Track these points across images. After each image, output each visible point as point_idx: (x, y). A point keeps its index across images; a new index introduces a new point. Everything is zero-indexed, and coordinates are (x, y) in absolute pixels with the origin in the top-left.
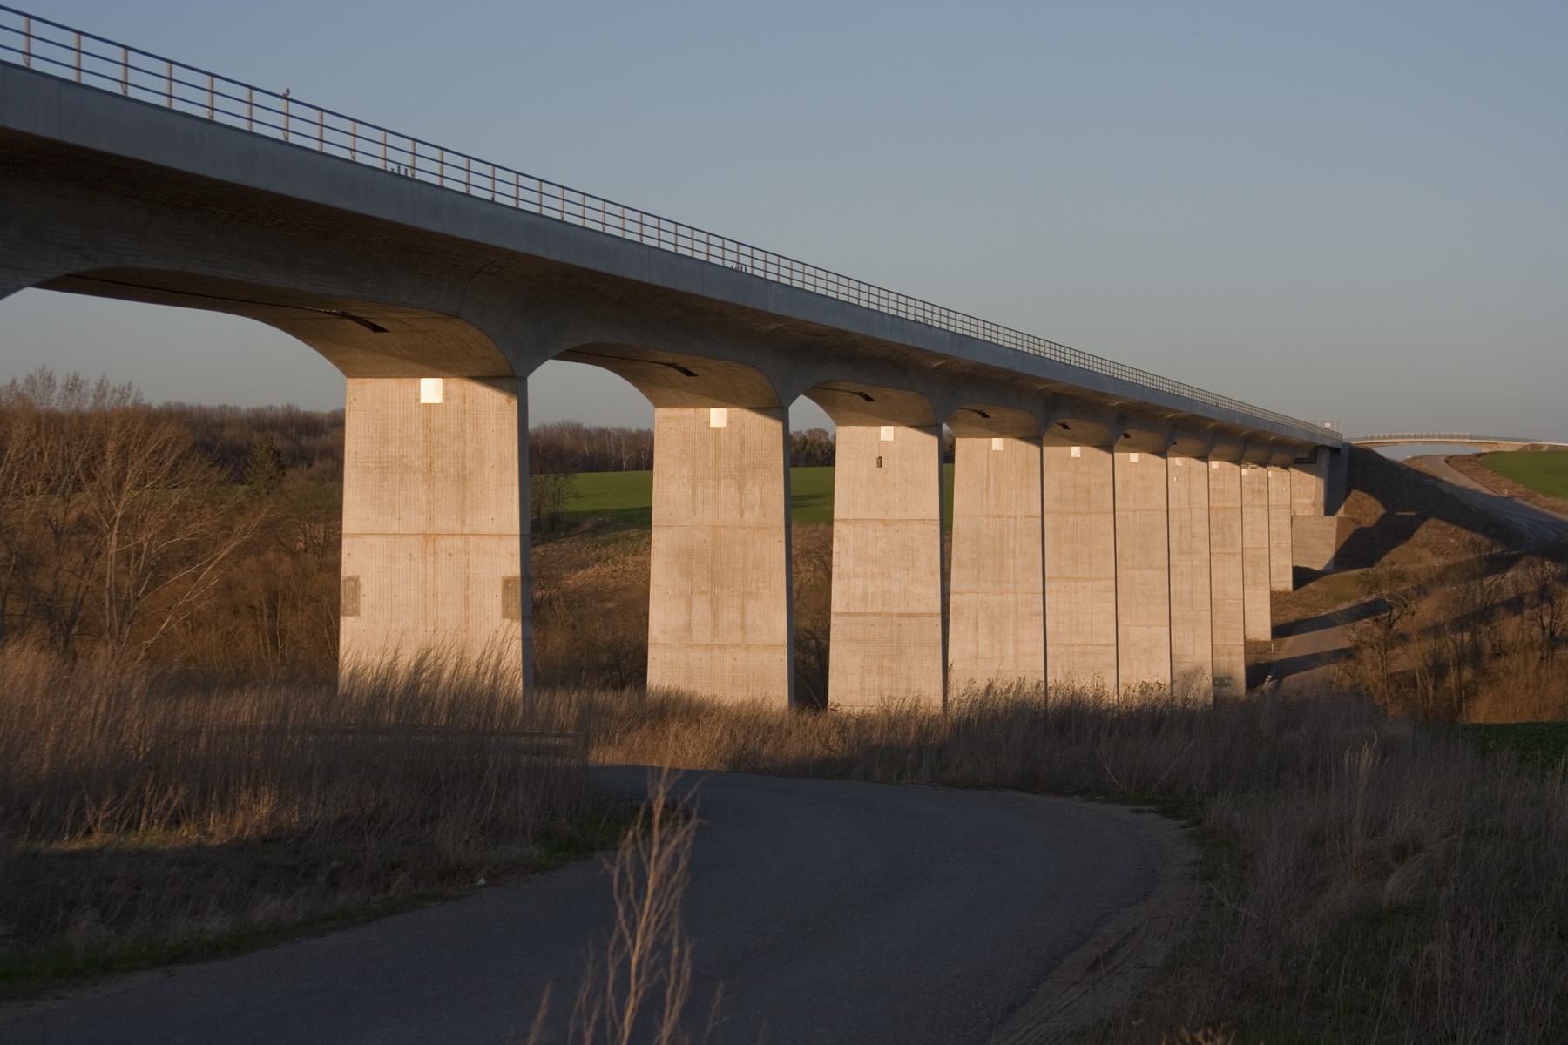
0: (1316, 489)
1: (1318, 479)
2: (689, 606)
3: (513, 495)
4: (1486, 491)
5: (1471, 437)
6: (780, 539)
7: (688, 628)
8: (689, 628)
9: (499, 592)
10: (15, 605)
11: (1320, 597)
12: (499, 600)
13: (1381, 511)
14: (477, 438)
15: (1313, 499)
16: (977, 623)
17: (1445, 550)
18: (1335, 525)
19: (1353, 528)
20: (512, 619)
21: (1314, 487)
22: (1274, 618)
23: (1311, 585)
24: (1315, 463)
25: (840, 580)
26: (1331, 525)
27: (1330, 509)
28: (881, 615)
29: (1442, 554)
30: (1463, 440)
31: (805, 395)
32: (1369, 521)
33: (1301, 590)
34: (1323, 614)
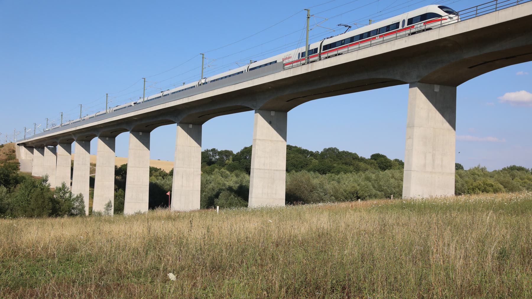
2: (425, 157)
7: (425, 166)
8: (425, 166)
10: (292, 173)
16: (183, 176)
22: (118, 177)
25: (257, 158)
28: (269, 170)
31: (419, 88)
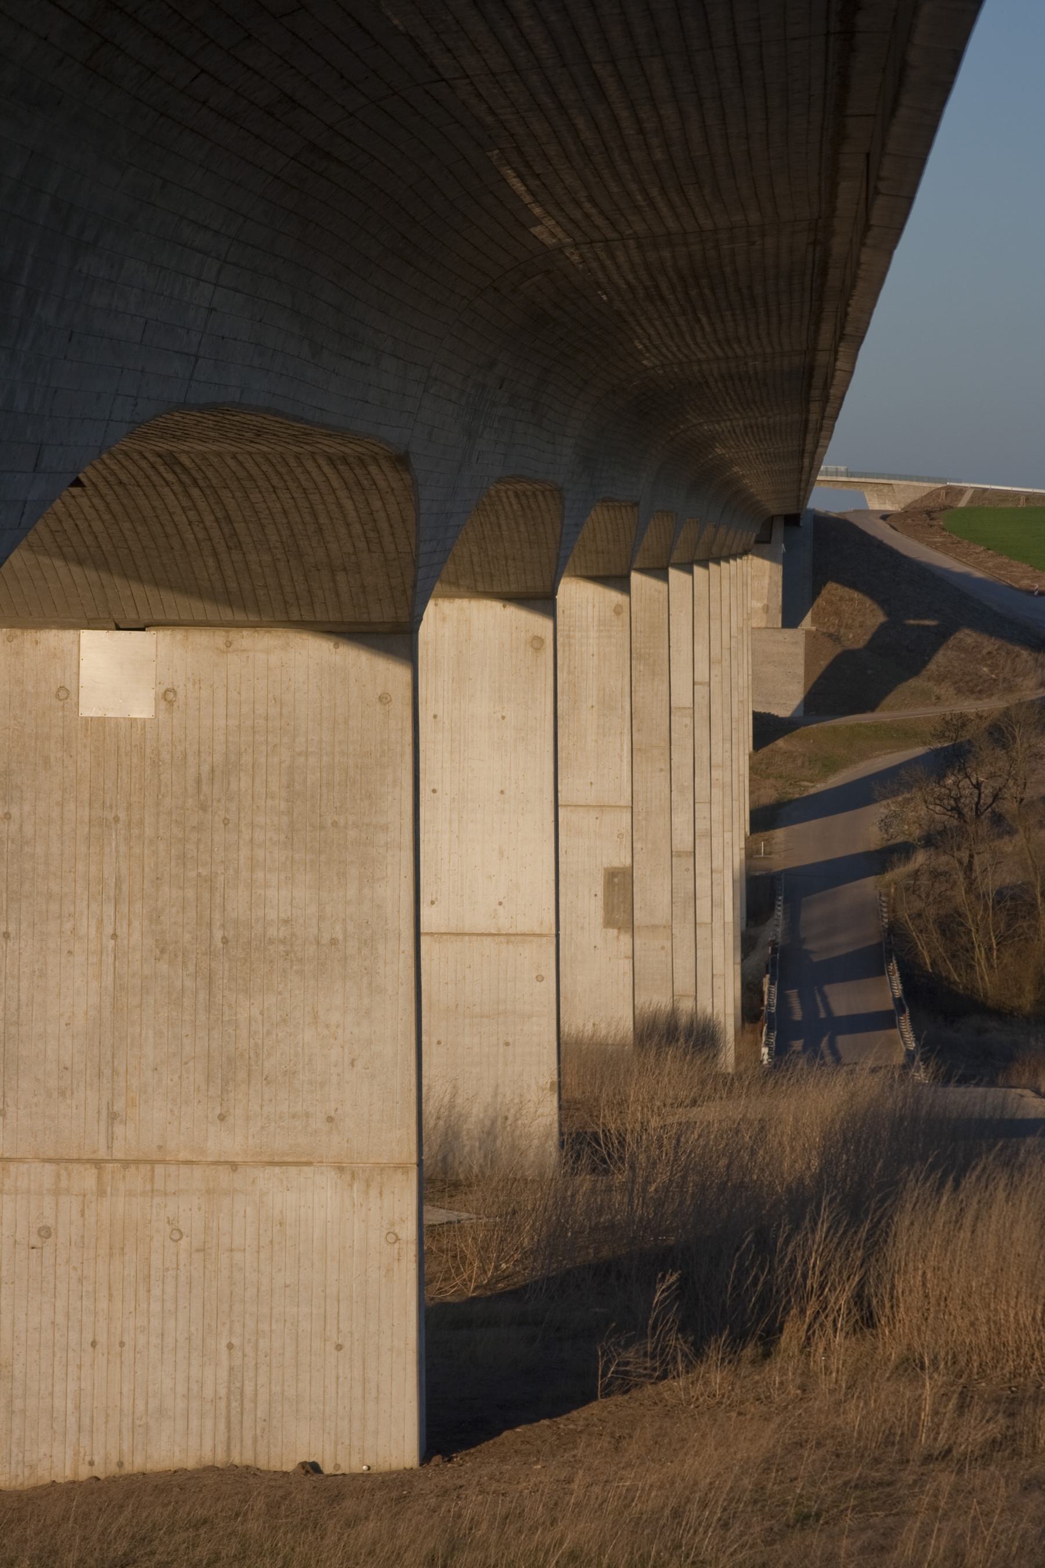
0: (769, 584)
1: (774, 565)
3: (622, 750)
4: (978, 574)
5: (848, 474)
6: (663, 766)
9: (599, 889)
11: (799, 762)
12: (600, 901)
13: (881, 618)
14: (569, 667)
15: (766, 602)
17: (977, 686)
18: (802, 645)
19: (829, 653)
20: (619, 929)
21: (766, 581)
23: (781, 743)
24: (769, 542)
26: (796, 643)
27: (790, 618)
29: (972, 692)
30: (834, 478)
32: (857, 638)
33: (765, 750)
34: (812, 791)
